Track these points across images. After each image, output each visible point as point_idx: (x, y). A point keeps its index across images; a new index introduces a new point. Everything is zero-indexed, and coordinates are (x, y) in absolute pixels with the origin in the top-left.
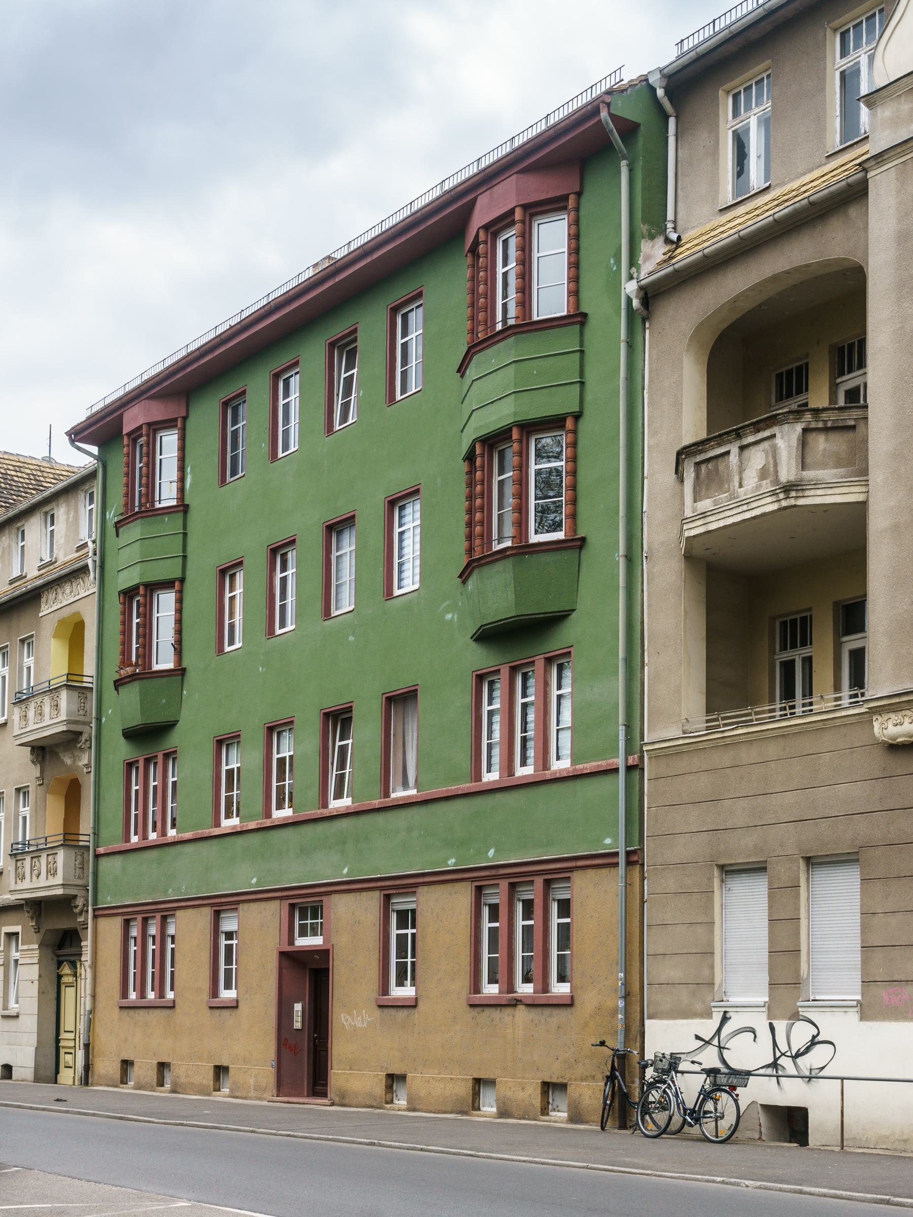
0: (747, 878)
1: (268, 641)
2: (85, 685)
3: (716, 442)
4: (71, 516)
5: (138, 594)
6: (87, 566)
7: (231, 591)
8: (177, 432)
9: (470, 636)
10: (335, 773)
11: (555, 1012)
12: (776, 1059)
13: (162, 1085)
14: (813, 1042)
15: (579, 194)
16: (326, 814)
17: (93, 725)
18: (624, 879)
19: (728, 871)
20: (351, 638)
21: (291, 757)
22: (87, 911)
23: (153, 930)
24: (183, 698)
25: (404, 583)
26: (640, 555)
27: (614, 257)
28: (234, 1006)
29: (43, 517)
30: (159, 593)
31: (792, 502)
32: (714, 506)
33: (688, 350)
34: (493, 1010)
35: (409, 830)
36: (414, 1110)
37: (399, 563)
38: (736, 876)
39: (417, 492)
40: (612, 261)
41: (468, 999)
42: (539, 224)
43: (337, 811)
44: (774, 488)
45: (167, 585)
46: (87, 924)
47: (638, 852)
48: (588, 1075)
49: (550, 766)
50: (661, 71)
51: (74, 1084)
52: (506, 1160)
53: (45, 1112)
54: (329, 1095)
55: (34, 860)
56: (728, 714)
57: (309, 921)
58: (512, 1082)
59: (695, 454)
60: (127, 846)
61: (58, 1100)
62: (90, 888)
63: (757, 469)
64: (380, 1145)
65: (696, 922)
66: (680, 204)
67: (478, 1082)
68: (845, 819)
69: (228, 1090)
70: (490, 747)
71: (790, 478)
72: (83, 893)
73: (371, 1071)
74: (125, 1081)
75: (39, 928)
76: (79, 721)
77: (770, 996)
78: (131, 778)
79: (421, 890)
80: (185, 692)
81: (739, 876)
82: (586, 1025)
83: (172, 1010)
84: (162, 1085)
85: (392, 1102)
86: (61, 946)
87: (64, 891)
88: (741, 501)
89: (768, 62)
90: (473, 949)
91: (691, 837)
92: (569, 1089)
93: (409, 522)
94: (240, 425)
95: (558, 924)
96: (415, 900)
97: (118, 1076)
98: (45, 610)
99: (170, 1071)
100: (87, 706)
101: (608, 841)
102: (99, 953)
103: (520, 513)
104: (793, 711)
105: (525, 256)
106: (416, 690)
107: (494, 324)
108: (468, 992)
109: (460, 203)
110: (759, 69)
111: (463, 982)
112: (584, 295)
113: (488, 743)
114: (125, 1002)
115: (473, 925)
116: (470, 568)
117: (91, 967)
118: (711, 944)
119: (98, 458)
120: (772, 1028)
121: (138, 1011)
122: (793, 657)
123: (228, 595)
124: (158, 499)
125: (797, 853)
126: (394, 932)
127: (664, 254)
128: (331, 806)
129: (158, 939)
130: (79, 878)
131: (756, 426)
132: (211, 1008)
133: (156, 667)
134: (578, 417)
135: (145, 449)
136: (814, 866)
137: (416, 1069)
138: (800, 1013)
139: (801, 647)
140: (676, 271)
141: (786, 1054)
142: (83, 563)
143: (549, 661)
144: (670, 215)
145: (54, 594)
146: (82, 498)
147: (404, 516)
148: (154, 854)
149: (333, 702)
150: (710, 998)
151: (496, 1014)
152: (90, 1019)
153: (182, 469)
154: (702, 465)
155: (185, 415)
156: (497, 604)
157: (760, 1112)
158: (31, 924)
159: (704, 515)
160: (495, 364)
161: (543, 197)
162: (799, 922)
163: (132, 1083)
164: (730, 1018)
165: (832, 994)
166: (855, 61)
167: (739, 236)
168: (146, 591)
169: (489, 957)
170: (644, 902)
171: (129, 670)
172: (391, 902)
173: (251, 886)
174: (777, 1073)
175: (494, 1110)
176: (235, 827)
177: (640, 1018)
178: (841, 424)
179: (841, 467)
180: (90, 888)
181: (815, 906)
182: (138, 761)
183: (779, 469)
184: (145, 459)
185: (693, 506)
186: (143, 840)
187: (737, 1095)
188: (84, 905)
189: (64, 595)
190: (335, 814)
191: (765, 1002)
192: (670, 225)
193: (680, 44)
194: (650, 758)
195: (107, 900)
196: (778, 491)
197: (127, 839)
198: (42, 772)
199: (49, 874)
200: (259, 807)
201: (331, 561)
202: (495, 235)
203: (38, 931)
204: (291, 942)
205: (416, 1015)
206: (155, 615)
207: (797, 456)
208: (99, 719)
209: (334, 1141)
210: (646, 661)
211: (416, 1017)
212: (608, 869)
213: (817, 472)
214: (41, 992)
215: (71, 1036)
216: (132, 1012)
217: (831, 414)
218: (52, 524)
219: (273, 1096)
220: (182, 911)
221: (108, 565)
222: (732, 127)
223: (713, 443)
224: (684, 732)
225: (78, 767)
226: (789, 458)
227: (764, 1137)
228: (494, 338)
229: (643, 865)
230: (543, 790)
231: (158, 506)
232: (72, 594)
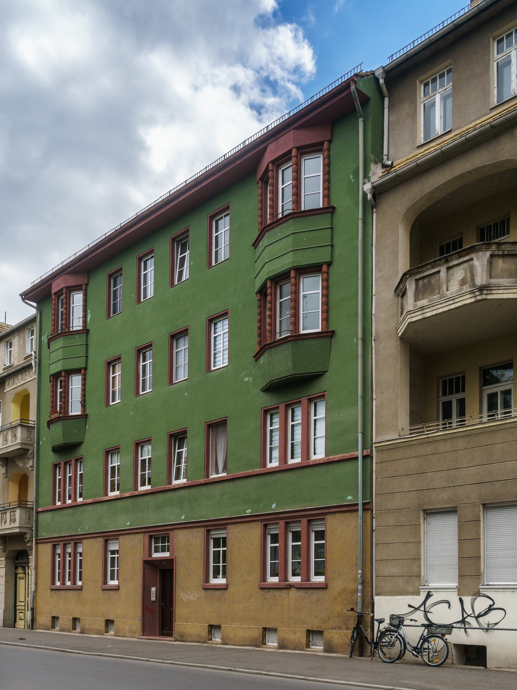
0: (440, 517)
1: (136, 398)
2: (30, 425)
3: (431, 266)
4: (21, 342)
5: (61, 376)
6: (31, 364)
7: (113, 374)
8: (82, 292)
9: (260, 389)
10: (175, 466)
11: (315, 592)
12: (464, 619)
13: (75, 629)
14: (490, 609)
15: (330, 141)
16: (171, 487)
17: (35, 446)
18: (361, 518)
19: (429, 513)
20: (186, 394)
21: (150, 459)
22: (32, 541)
23: (69, 550)
24: (86, 430)
25: (217, 364)
26: (370, 339)
27: (353, 174)
28: (116, 589)
29: (5, 344)
30: (72, 376)
31: (484, 297)
32: (429, 303)
33: (401, 222)
34: (275, 591)
35: (222, 495)
36: (226, 644)
37: (214, 353)
38: (433, 516)
39: (226, 314)
40: (351, 177)
41: (260, 585)
42: (305, 160)
43: (178, 486)
44: (473, 289)
45: (77, 371)
46: (32, 547)
47: (370, 503)
48: (336, 626)
49: (310, 458)
50: (383, 68)
51: (25, 628)
52: (330, 683)
53: (15, 646)
54: (174, 636)
55: (3, 515)
56: (431, 425)
57: (160, 545)
58: (288, 630)
59: (416, 274)
60: (54, 507)
61: (21, 639)
62: (34, 529)
63: (458, 280)
64: (236, 671)
65: (408, 541)
66: (390, 146)
67: (265, 629)
68: (513, 481)
69: (113, 632)
70: (271, 449)
71: (483, 283)
72: (30, 531)
73: (199, 623)
74: (54, 627)
75: (5, 550)
76: (27, 443)
77: (459, 583)
78: (56, 473)
79: (229, 527)
80: (87, 427)
81: (435, 515)
82: (335, 599)
83: (81, 591)
84: (75, 629)
85: (211, 640)
86: (17, 558)
87: (20, 530)
88: (449, 298)
89: (449, 61)
90: (262, 558)
91: (405, 494)
92: (325, 634)
93: (220, 331)
94: (118, 287)
95: (292, 545)
96: (226, 532)
97: (50, 624)
98: (7, 389)
99: (79, 622)
100: (32, 436)
101: (350, 498)
102: (39, 562)
103: (295, 318)
104: (481, 420)
105: (298, 176)
106: (226, 420)
107: (277, 214)
108: (259, 581)
109: (257, 150)
110: (442, 66)
111: (256, 575)
112: (333, 197)
113: (270, 447)
114: (53, 587)
115: (262, 545)
116: (264, 350)
117: (34, 569)
118: (419, 554)
119: (37, 308)
120: (461, 601)
121: (61, 592)
122: (451, 399)
123: (111, 376)
124: (72, 326)
125: (478, 501)
126: (212, 549)
127: (382, 173)
128: (173, 484)
129: (62, 556)
130: (28, 524)
131: (460, 254)
132: (103, 590)
133: (71, 414)
134: (329, 264)
135: (64, 300)
136: (487, 509)
137: (227, 622)
138: (481, 592)
139: (455, 393)
140: (397, 176)
141: (471, 615)
142: (29, 362)
143: (310, 400)
144: (385, 152)
145: (13, 380)
146: (27, 333)
147: (217, 328)
148: (70, 511)
149: (175, 428)
150: (418, 584)
151: (277, 593)
152: (34, 595)
153: (85, 311)
154: (420, 281)
155: (87, 283)
156: (281, 369)
157: (453, 648)
158: (1, 548)
159: (422, 308)
160: (279, 236)
161: (309, 142)
162: (480, 540)
163: (58, 628)
164: (432, 595)
165: (496, 581)
166: (508, 55)
167: (441, 150)
168: (65, 374)
169: (271, 563)
170: (373, 531)
171: (56, 415)
172: (210, 533)
173: (126, 526)
174: (464, 626)
175: (276, 644)
176: (117, 496)
177: (371, 595)
178: (513, 253)
179: (512, 278)
180: (34, 529)
181: (488, 532)
182: (60, 463)
183: (476, 278)
184: (64, 306)
185: (414, 304)
186: (64, 504)
187: (446, 639)
188: (30, 538)
189: (18, 380)
190: (177, 487)
191: (457, 586)
192: (385, 157)
193: (391, 58)
194: (377, 451)
195: (43, 535)
196: (475, 291)
197: (55, 504)
198: (6, 471)
199: (11, 522)
200: (131, 485)
201: (173, 354)
202: (278, 167)
203: (4, 551)
204: (150, 555)
205: (226, 593)
206: (70, 387)
207: (487, 270)
208: (38, 443)
209: (203, 668)
210: (374, 397)
211: (227, 594)
212: (350, 513)
213: (499, 280)
214: (7, 582)
215: (23, 604)
216: (58, 592)
217: (508, 247)
218: (11, 347)
219: (140, 636)
220: (86, 540)
221: (43, 364)
222: (424, 102)
223: (429, 266)
224: (400, 436)
225: (27, 468)
226: (483, 271)
227: (454, 662)
228: (277, 223)
229: (372, 510)
230: (307, 471)
231: (71, 329)
232: (23, 380)
